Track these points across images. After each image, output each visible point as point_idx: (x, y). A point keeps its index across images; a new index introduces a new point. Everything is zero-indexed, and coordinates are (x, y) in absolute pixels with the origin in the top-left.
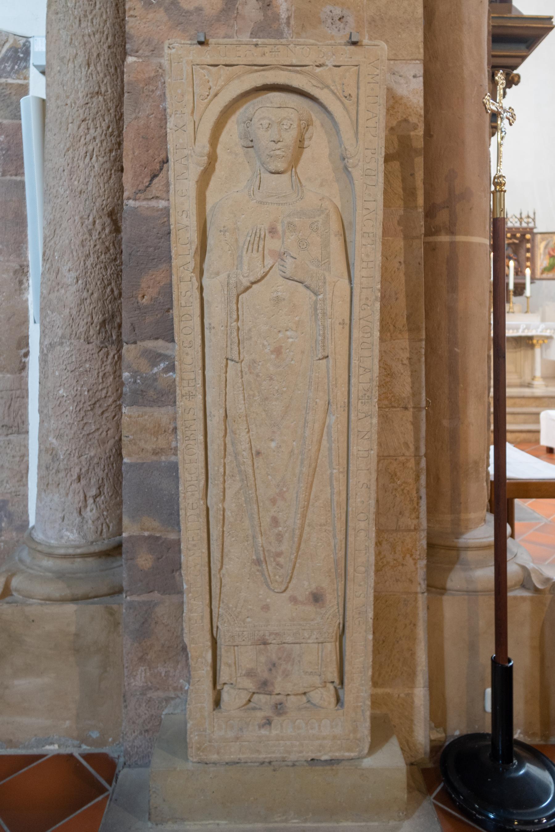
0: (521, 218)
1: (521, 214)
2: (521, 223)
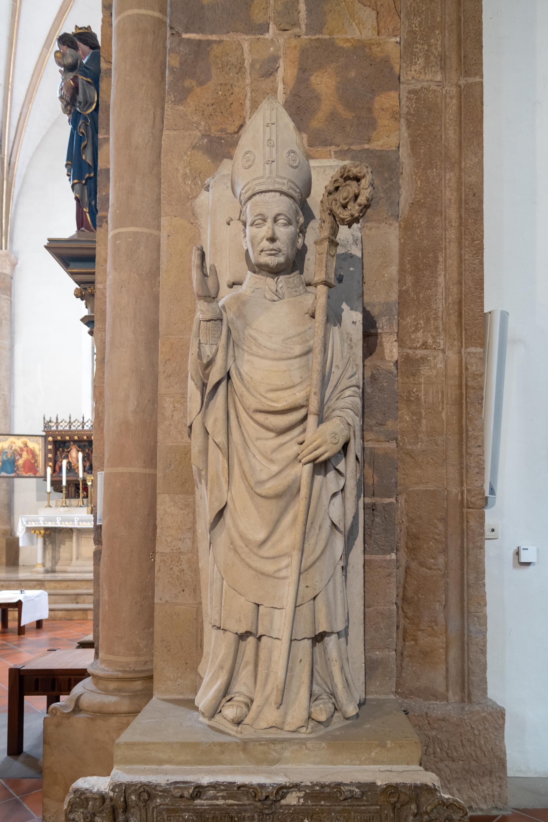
0: (83, 422)
1: (57, 419)
2: (70, 427)
